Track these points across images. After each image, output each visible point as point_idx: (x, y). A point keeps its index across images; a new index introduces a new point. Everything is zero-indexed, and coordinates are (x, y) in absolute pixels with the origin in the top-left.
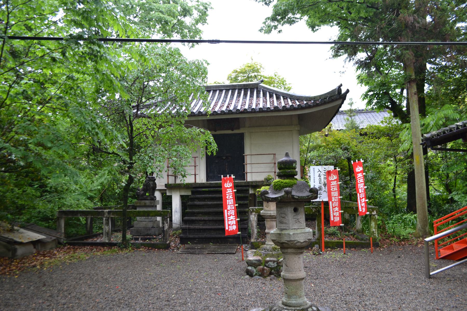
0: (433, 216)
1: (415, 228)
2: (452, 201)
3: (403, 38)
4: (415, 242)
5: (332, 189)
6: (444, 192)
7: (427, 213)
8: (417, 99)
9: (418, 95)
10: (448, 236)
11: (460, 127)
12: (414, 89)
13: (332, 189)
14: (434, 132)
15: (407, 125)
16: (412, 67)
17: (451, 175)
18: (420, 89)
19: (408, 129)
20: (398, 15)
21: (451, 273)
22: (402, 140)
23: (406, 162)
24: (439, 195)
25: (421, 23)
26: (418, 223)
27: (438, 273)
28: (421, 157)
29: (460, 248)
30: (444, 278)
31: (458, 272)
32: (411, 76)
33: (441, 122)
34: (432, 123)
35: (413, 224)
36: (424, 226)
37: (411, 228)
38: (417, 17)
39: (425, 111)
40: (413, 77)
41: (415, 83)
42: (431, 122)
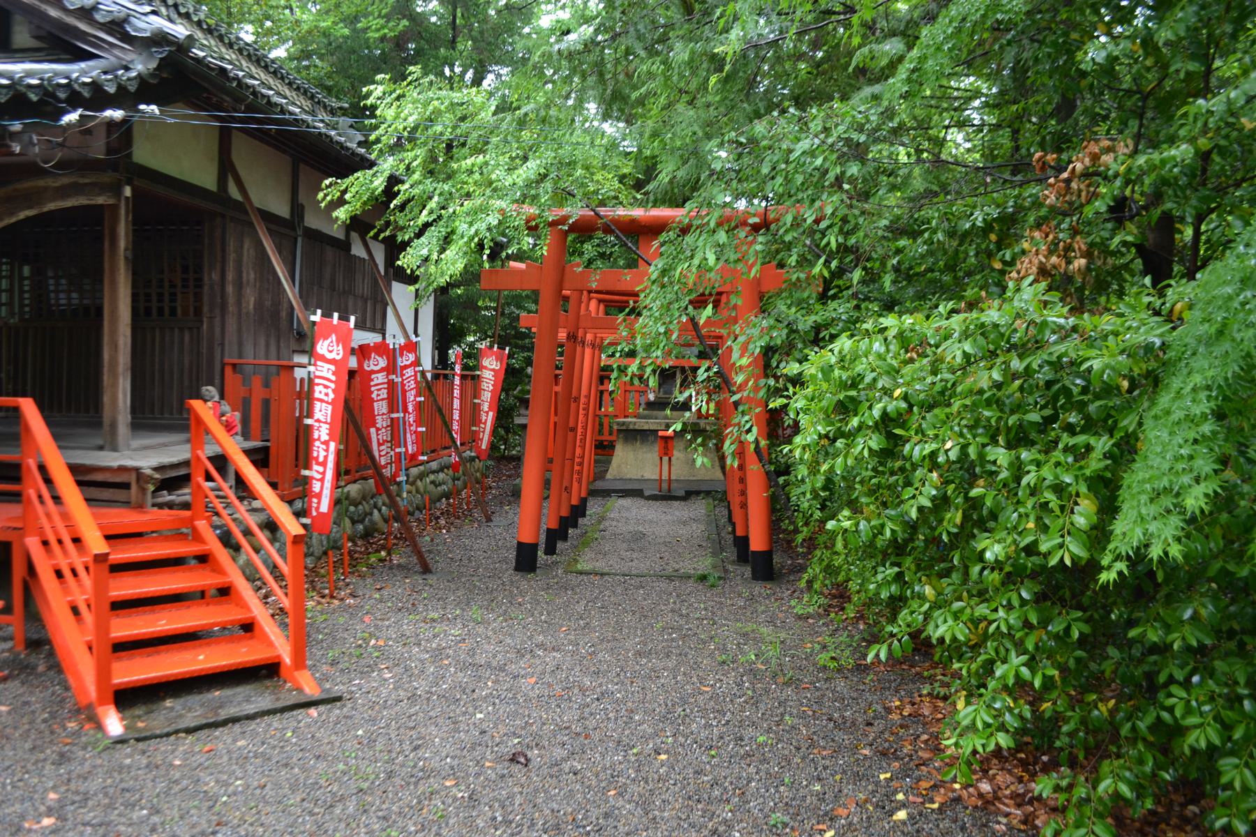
5: (374, 396)
13: (374, 396)
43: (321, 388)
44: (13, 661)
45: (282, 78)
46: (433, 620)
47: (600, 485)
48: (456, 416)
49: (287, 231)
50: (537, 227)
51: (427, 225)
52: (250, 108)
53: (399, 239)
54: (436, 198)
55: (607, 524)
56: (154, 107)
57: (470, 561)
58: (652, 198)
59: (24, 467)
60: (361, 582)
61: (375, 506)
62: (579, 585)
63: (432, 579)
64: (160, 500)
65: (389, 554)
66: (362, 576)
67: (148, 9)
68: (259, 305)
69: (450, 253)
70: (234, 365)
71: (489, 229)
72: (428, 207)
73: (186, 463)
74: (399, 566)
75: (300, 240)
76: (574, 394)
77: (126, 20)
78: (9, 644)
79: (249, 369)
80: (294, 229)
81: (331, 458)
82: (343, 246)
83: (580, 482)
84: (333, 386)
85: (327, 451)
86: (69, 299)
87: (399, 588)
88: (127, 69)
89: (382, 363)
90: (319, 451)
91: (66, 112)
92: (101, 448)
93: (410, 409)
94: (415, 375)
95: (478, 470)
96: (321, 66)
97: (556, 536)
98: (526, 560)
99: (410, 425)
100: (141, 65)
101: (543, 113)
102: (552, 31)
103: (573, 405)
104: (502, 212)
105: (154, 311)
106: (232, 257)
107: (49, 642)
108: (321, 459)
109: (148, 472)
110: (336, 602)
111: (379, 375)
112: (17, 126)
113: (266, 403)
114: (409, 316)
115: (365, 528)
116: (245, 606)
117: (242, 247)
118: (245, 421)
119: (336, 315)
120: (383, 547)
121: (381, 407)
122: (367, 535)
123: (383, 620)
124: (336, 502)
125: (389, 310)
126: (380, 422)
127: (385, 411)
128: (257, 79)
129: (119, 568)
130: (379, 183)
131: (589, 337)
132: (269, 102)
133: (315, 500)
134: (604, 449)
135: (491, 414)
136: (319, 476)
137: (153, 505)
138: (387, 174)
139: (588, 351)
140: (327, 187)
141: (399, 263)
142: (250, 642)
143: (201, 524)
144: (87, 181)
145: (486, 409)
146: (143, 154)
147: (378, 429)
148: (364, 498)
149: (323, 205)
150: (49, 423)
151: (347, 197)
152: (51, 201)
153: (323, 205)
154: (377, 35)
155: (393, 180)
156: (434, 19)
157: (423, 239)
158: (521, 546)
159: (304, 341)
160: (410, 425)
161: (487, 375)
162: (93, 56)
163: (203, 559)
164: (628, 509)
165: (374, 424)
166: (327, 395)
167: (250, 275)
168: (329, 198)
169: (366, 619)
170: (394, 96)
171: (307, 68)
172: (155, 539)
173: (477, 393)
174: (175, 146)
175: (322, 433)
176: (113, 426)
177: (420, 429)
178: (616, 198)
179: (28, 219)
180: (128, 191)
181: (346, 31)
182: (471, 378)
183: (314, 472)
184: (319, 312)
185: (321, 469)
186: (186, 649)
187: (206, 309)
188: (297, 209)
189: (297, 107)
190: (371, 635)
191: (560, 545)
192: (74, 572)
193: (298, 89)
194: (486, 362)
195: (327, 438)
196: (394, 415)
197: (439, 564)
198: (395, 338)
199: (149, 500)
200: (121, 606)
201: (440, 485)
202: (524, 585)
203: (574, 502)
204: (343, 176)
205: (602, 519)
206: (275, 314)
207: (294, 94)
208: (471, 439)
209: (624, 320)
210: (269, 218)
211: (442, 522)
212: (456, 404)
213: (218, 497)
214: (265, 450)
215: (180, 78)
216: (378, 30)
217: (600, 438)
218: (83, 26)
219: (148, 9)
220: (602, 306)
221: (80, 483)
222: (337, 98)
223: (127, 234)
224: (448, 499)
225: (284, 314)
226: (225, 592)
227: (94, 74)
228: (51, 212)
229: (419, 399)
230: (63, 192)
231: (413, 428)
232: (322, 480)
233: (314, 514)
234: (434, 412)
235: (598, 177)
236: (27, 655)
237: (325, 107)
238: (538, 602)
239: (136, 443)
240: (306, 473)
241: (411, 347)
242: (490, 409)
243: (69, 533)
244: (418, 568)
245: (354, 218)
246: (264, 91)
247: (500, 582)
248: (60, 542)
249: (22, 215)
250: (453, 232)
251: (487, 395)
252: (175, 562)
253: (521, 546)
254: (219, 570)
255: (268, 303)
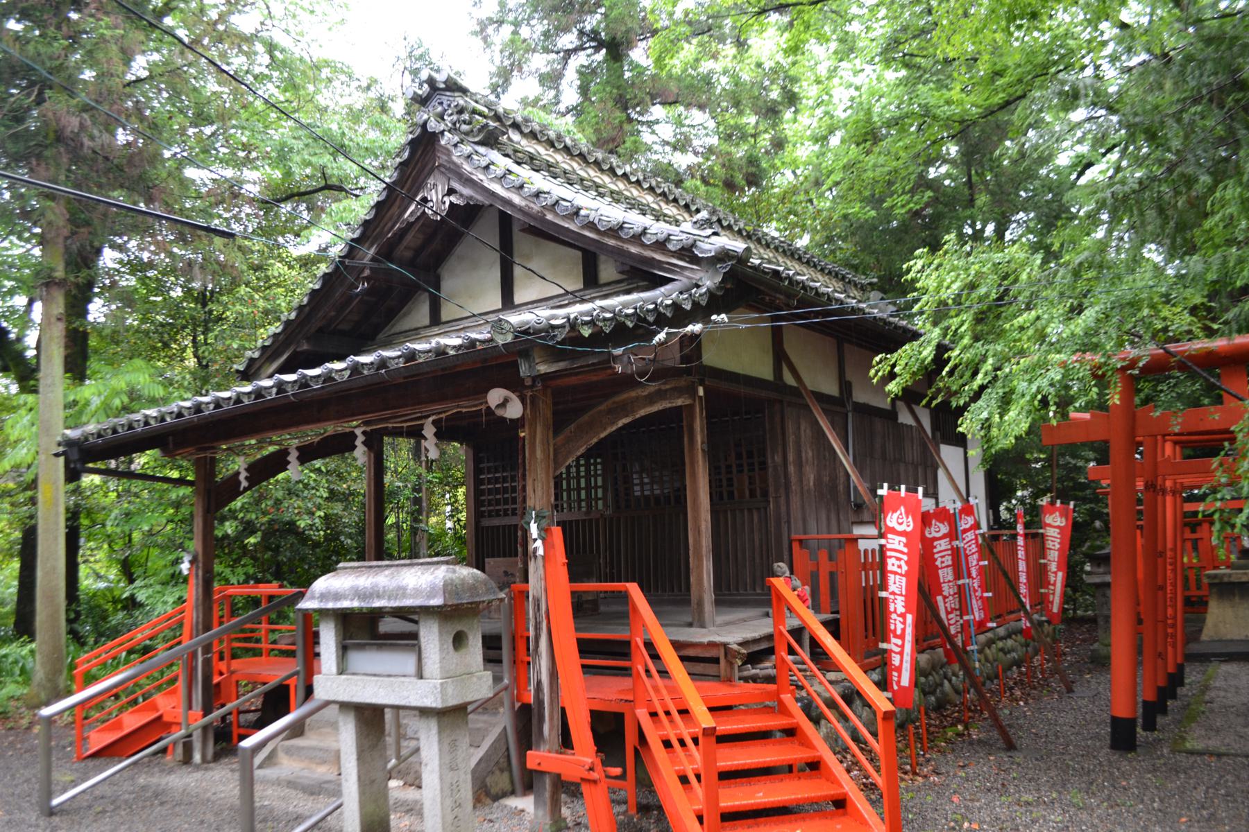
0: (83, 644)
1: (27, 682)
2: (132, 604)
3: (43, 165)
4: (25, 722)
5: (938, 563)
6: (119, 581)
7: (64, 637)
8: (64, 333)
9: (70, 323)
10: (113, 693)
11: (152, 422)
12: (59, 307)
13: (938, 563)
14: (92, 428)
15: (30, 398)
16: (61, 249)
17: (136, 536)
18: (77, 306)
19: (31, 410)
20: (40, 101)
21: (109, 793)
22: (12, 438)
23: (21, 498)
24: (107, 588)
25: (99, 141)
26: (38, 667)
27: (74, 797)
28: (57, 489)
29: (139, 724)
30: (90, 807)
31: (127, 786)
32: (52, 270)
33: (117, 402)
34: (96, 402)
35: (23, 671)
36: (54, 673)
37: (17, 682)
38: (89, 122)
39: (84, 369)
40: (60, 273)
41: (63, 291)
42: (95, 398)
43: (893, 560)
44: (628, 824)
45: (815, 266)
46: (1028, 803)
47: (1194, 648)
48: (1023, 579)
49: (838, 409)
50: (1104, 375)
51: (982, 388)
52: (803, 303)
53: (954, 404)
54: (990, 361)
55: (1213, 694)
56: (723, 316)
57: (1058, 738)
58: (1235, 327)
59: (633, 645)
60: (942, 759)
61: (946, 677)
62: (1192, 768)
63: (1019, 758)
64: (745, 673)
65: (966, 728)
66: (942, 752)
67: (709, 231)
68: (818, 480)
69: (1012, 414)
70: (801, 541)
71: (1052, 385)
72: (983, 371)
73: (769, 637)
74: (980, 741)
75: (850, 415)
76: (1160, 548)
77: (694, 245)
78: (623, 808)
79: (813, 544)
80: (844, 406)
81: (909, 630)
82: (891, 415)
83: (1174, 646)
84: (905, 558)
85: (904, 623)
86: (652, 490)
87: (984, 766)
88: (698, 286)
89: (944, 529)
90: (896, 624)
91: (655, 333)
92: (690, 625)
93: (974, 573)
94: (976, 539)
95: (1047, 636)
96: (847, 248)
97: (1153, 710)
98: (1123, 737)
99: (975, 591)
100: (709, 281)
101: (1098, 258)
102: (1073, 166)
103: (1160, 560)
104: (1063, 364)
105: (725, 495)
106: (791, 439)
107: (660, 808)
108: (899, 632)
109: (735, 647)
110: (920, 779)
111: (942, 542)
112: (618, 351)
113: (832, 575)
114: (960, 476)
115: (937, 699)
116: (834, 781)
117: (799, 428)
118: (814, 593)
119: (903, 487)
120: (959, 721)
121: (946, 574)
122: (940, 707)
123: (972, 800)
124: (918, 671)
125: (941, 473)
126: (947, 589)
127: (951, 578)
128: (790, 268)
129: (725, 739)
130: (928, 353)
131: (1168, 484)
132: (817, 293)
133: (895, 674)
134: (1196, 606)
135: (1060, 574)
136: (898, 650)
137: (740, 679)
138: (934, 343)
139: (1169, 499)
140: (878, 363)
141: (960, 429)
142: (842, 818)
143: (787, 698)
144: (668, 387)
145: (1054, 569)
146: (711, 357)
147: (945, 597)
148: (934, 668)
149: (875, 381)
150: (651, 603)
151: (897, 370)
152: (640, 408)
153: (875, 381)
154: (903, 211)
155: (941, 349)
156: (947, 182)
157: (980, 403)
158: (1115, 721)
159: (874, 514)
160: (975, 591)
161: (1052, 533)
162: (674, 280)
163: (791, 732)
164: (1235, 676)
165: (940, 592)
166: (900, 567)
167: (808, 453)
168: (880, 374)
169: (955, 799)
170: (933, 267)
171: (833, 252)
172: (745, 712)
173: (1043, 551)
174: (736, 344)
175: (898, 605)
176: (700, 604)
177: (986, 595)
178: (1189, 332)
179: (625, 426)
180: (701, 392)
181: (873, 213)
182: (1036, 540)
183: (893, 645)
184: (886, 485)
185: (899, 642)
186: (783, 822)
187: (771, 489)
188: (846, 387)
189: (825, 285)
190: (964, 817)
191: (1160, 720)
192: (682, 743)
193: (830, 273)
194: (1049, 519)
195: (903, 610)
196: (960, 582)
197: (1024, 740)
198: (949, 499)
199: (737, 674)
200: (728, 776)
201: (1009, 652)
202: (1125, 766)
203: (1171, 669)
204: (892, 351)
205: (1206, 688)
206: (833, 488)
207: (826, 278)
208: (1041, 601)
209: (1221, 465)
210: (821, 398)
211: (1018, 693)
212: (1022, 566)
213: (800, 670)
214: (836, 621)
215: (742, 286)
216: (903, 206)
217: (1187, 593)
218: (658, 257)
219: (709, 231)
220: (1178, 448)
221: (683, 659)
222: (864, 274)
223: (702, 430)
224: (1019, 667)
225: (841, 488)
226: (815, 766)
227: (674, 296)
228: (642, 418)
229: (982, 563)
230: (651, 399)
231: (979, 594)
232: (901, 653)
233: (896, 687)
234: (1000, 576)
235: (1165, 312)
236: (639, 819)
237: (856, 285)
238: (1147, 788)
239: (720, 619)
240: (884, 646)
241: (968, 510)
242: (1059, 569)
243: (675, 705)
244: (1001, 744)
245: (905, 390)
246: (812, 284)
247: (1096, 762)
248: (668, 713)
249: (620, 424)
250: (1012, 391)
251: (1053, 555)
252: (763, 736)
253: (1115, 721)
254: (807, 743)
255: (826, 479)
